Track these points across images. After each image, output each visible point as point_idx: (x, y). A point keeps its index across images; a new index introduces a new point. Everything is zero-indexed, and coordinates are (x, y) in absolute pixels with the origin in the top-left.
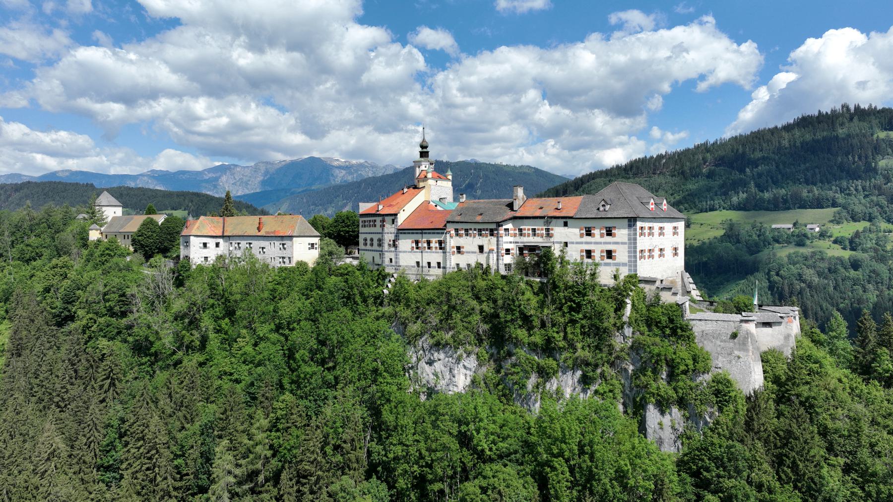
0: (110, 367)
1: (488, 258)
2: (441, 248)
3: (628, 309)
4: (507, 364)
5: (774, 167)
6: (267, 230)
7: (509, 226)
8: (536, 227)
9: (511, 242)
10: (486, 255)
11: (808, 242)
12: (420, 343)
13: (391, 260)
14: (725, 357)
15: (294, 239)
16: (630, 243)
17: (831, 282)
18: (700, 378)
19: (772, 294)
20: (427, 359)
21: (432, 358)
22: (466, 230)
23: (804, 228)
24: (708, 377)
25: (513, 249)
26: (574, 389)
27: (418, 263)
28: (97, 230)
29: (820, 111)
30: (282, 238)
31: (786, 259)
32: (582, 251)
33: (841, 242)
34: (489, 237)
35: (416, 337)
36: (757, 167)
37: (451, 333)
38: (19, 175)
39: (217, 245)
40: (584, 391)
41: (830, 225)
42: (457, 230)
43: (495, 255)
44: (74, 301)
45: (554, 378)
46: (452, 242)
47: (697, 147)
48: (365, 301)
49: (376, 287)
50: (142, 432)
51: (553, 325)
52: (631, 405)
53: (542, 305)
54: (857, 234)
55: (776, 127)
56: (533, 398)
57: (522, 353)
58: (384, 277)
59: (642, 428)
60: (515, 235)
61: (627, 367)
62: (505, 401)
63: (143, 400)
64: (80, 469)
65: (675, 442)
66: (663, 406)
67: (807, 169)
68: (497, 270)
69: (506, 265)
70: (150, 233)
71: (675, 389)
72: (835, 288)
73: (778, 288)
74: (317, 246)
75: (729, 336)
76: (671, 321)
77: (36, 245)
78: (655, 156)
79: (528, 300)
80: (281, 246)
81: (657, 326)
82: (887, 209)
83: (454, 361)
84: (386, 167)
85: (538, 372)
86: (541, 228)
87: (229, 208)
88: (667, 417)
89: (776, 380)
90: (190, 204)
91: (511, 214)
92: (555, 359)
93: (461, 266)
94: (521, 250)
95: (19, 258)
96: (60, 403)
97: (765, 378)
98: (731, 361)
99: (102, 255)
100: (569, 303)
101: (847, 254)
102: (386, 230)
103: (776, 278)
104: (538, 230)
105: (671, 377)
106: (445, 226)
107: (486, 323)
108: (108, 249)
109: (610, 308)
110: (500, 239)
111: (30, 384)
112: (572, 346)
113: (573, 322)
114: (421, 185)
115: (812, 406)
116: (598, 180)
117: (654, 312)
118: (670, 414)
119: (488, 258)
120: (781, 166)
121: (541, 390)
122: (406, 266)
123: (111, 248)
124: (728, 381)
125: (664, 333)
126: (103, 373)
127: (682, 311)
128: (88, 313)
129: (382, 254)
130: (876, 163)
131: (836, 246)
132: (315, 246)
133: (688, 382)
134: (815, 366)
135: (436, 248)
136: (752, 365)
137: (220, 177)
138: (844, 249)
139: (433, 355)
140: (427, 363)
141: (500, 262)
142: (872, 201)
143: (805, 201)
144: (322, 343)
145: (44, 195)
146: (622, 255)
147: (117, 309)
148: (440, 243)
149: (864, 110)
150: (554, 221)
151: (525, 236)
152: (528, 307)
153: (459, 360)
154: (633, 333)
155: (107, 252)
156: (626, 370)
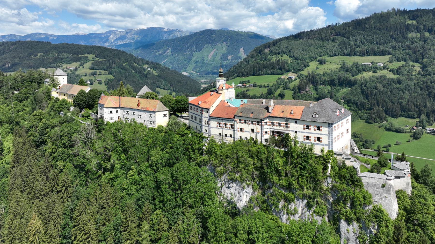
0: (65, 181)
1: (256, 136)
2: (232, 128)
3: (329, 170)
4: (268, 193)
5: (362, 37)
6: (142, 107)
7: (267, 120)
8: (281, 122)
9: (268, 128)
10: (255, 134)
11: (378, 71)
12: (223, 177)
13: (206, 130)
14: (379, 196)
15: (156, 113)
16: (329, 135)
17: (389, 90)
18: (367, 208)
19: (363, 95)
20: (227, 185)
21: (229, 186)
22: (245, 121)
23: (376, 64)
24: (371, 207)
25: (269, 132)
26: (303, 209)
27: (220, 134)
28: (55, 91)
29: (382, 11)
30: (150, 112)
31: (369, 79)
32: (304, 136)
33: (392, 71)
34: (257, 126)
35: (221, 174)
36: (355, 36)
37: (239, 174)
38: (14, 35)
39: (117, 111)
40: (308, 211)
41: (388, 63)
42: (240, 120)
43: (260, 135)
44: (45, 134)
45: (293, 202)
46: (238, 126)
47: (328, 27)
48: (194, 151)
49: (199, 143)
50: (83, 227)
51: (292, 176)
52: (331, 217)
53: (285, 164)
54: (400, 68)
55: (363, 18)
56: (282, 212)
57: (276, 189)
58: (203, 138)
59: (338, 231)
60: (270, 125)
61: (330, 198)
62: (268, 213)
63: (83, 205)
64: (51, 240)
65: (356, 240)
66: (349, 221)
67: (377, 38)
68: (261, 142)
69: (265, 139)
70: (82, 98)
71: (355, 213)
72: (391, 92)
73: (365, 92)
74: (167, 115)
75: (381, 186)
76: (352, 177)
77: (25, 93)
78: (309, 31)
79: (278, 161)
80: (149, 116)
81: (344, 178)
82: (412, 56)
83: (241, 189)
84: (186, 32)
85: (285, 199)
86: (283, 123)
87: (122, 90)
88: (351, 226)
89: (405, 209)
90: (96, 52)
91: (267, 114)
92: (293, 193)
93: (242, 138)
94: (273, 132)
95: (16, 100)
96: (39, 197)
97: (399, 207)
98: (382, 199)
99: (58, 108)
100: (300, 166)
101: (395, 77)
102: (203, 115)
103: (365, 88)
104: (282, 123)
105: (353, 206)
106: (234, 117)
107: (256, 170)
108: (61, 105)
109: (320, 168)
110: (263, 127)
111: (24, 181)
112: (302, 187)
113: (302, 175)
114: (220, 92)
115: (424, 226)
116: (283, 41)
117: (342, 171)
118: (353, 225)
119: (256, 136)
120: (366, 36)
121: (286, 208)
122: (214, 135)
123: (63, 104)
124: (382, 211)
125: (348, 182)
126: (61, 184)
127: (357, 172)
128: (53, 145)
129: (201, 126)
130: (407, 35)
131: (391, 73)
132: (166, 115)
133: (362, 210)
134: (423, 201)
135: (229, 127)
136: (392, 202)
137: (109, 36)
138: (394, 74)
139: (230, 184)
140: (227, 188)
141: (263, 138)
142: (406, 52)
143: (376, 52)
144: (175, 181)
145: (27, 47)
146: (325, 140)
147: (67, 144)
148: (232, 125)
149: (401, 11)
150: (290, 120)
151: (275, 126)
152: (279, 165)
153: (243, 188)
154: (332, 182)
155: (61, 106)
156: (329, 200)
